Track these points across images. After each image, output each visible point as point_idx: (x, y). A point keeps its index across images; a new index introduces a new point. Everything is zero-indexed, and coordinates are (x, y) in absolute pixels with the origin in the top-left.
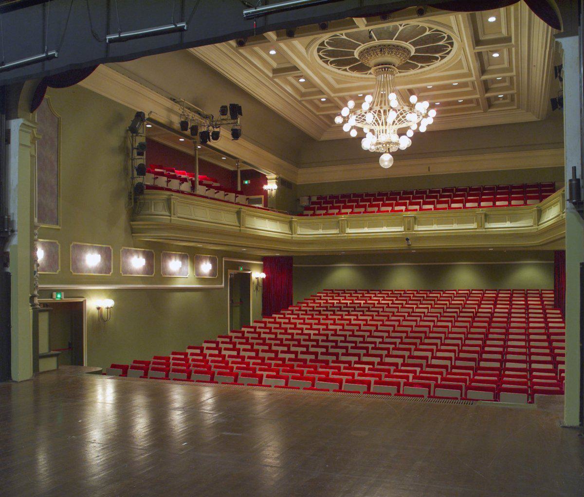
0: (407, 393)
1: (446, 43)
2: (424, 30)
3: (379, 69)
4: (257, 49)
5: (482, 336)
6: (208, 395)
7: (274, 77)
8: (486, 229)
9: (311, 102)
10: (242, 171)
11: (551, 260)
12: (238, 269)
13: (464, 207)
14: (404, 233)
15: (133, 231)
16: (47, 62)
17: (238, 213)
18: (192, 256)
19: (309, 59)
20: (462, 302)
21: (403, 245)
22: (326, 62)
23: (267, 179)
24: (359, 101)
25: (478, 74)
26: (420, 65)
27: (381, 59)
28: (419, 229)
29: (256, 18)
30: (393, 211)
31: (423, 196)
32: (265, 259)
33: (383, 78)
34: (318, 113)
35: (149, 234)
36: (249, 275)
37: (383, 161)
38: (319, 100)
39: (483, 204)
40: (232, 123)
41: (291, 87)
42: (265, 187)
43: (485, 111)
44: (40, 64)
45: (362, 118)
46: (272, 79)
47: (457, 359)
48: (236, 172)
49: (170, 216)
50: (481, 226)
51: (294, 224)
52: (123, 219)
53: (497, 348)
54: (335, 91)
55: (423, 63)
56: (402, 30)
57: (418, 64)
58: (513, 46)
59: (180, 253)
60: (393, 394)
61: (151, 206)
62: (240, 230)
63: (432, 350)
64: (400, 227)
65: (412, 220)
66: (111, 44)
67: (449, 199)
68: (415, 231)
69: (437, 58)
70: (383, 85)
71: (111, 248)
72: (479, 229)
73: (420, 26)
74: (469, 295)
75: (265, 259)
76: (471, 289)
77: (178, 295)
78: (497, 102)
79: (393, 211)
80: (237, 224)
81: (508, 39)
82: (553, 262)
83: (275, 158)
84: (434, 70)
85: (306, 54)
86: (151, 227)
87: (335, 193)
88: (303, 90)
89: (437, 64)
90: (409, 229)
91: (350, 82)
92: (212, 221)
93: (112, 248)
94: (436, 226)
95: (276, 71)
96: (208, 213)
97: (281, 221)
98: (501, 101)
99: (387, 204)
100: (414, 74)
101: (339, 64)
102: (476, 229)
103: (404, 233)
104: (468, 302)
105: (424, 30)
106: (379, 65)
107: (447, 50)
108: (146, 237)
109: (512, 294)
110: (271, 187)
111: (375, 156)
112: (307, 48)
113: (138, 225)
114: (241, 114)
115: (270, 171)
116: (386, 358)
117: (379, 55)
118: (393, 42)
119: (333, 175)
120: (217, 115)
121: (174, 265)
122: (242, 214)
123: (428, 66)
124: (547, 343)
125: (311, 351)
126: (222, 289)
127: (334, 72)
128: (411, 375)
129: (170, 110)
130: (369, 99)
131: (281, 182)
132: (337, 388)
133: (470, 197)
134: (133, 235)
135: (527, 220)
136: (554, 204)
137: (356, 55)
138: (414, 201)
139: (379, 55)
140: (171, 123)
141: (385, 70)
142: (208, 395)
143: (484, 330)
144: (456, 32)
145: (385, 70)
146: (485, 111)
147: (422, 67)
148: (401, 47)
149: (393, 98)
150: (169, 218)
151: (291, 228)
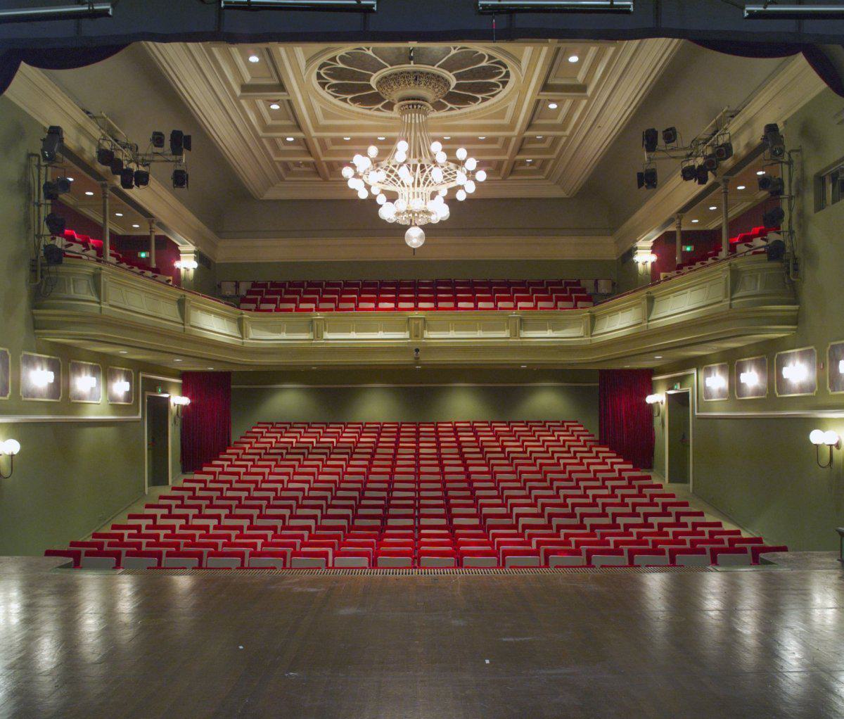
0: (253, 566)
1: (326, 79)
2: (482, 57)
3: (409, 105)
4: (215, 50)
5: (359, 485)
6: (183, 582)
7: (241, 97)
8: (521, 338)
9: (273, 141)
10: (156, 236)
11: (595, 382)
12: (156, 391)
13: (476, 308)
14: (409, 341)
15: (36, 325)
16: (85, 22)
17: (181, 303)
18: (106, 368)
19: (305, 77)
20: (354, 440)
21: (407, 359)
22: (323, 85)
23: (179, 252)
24: (387, 148)
25: (524, 128)
26: (450, 106)
27: (412, 91)
28: (431, 336)
29: (495, 13)
30: (297, 309)
31: (281, 291)
32: (185, 376)
33: (409, 119)
34: (275, 159)
35: (66, 332)
36: (167, 400)
37: (410, 238)
38: (284, 139)
39: (421, 305)
40: (173, 161)
41: (255, 113)
42: (177, 264)
43: (504, 179)
44: (72, 22)
45: (392, 175)
46: (237, 99)
47: (325, 517)
48: (148, 238)
49: (99, 303)
50: (515, 334)
51: (246, 323)
52: (23, 303)
53: (601, 494)
54: (318, 128)
55: (454, 104)
56: (453, 55)
57: (448, 104)
58: (586, 97)
59: (91, 364)
60: (234, 567)
61: (69, 286)
62: (184, 329)
63: (290, 507)
64: (403, 333)
65: (421, 323)
66: (227, 12)
67: (317, 296)
68: (425, 339)
69: (475, 100)
70: (423, 127)
71: (8, 353)
72: (512, 339)
73: (480, 53)
74: (380, 430)
75: (185, 376)
76: (471, 421)
77: (89, 431)
78: (522, 168)
79: (496, 308)
80: (179, 320)
81: (582, 88)
82: (598, 384)
83: (195, 219)
84: (466, 116)
85: (304, 68)
86: (70, 319)
87: (279, 279)
88: (269, 121)
89: (473, 107)
90: (417, 336)
91: (347, 119)
92: (151, 313)
93: (10, 352)
94: (454, 333)
95: (245, 88)
96: (134, 298)
97: (229, 318)
98: (527, 167)
99: (248, 299)
100: (437, 118)
101: (339, 90)
102: (509, 338)
103: (409, 341)
104: (362, 440)
105: (482, 57)
106: (409, 99)
107: (495, 90)
108: (60, 336)
109: (399, 429)
110: (187, 264)
111: (399, 230)
112: (310, 61)
113: (45, 315)
114: (189, 148)
115: (189, 241)
116: (291, 520)
117: (412, 85)
118: (435, 69)
119: (274, 251)
120: (146, 147)
121: (85, 383)
122: (187, 305)
123: (459, 108)
124: (441, 492)
125: (176, 513)
126: (138, 422)
127: (328, 101)
128: (259, 542)
129: (81, 129)
130: (402, 147)
131: (200, 257)
132: (197, 565)
133: (364, 294)
134: (36, 331)
135: (574, 329)
136: (624, 309)
137: (373, 82)
138: (267, 297)
139: (412, 85)
140: (82, 150)
141: (413, 107)
142: (126, 586)
143: (361, 478)
144: (523, 70)
145: (413, 107)
146: (504, 179)
147: (451, 109)
148: (443, 78)
149: (436, 147)
150: (98, 305)
151: (241, 329)
